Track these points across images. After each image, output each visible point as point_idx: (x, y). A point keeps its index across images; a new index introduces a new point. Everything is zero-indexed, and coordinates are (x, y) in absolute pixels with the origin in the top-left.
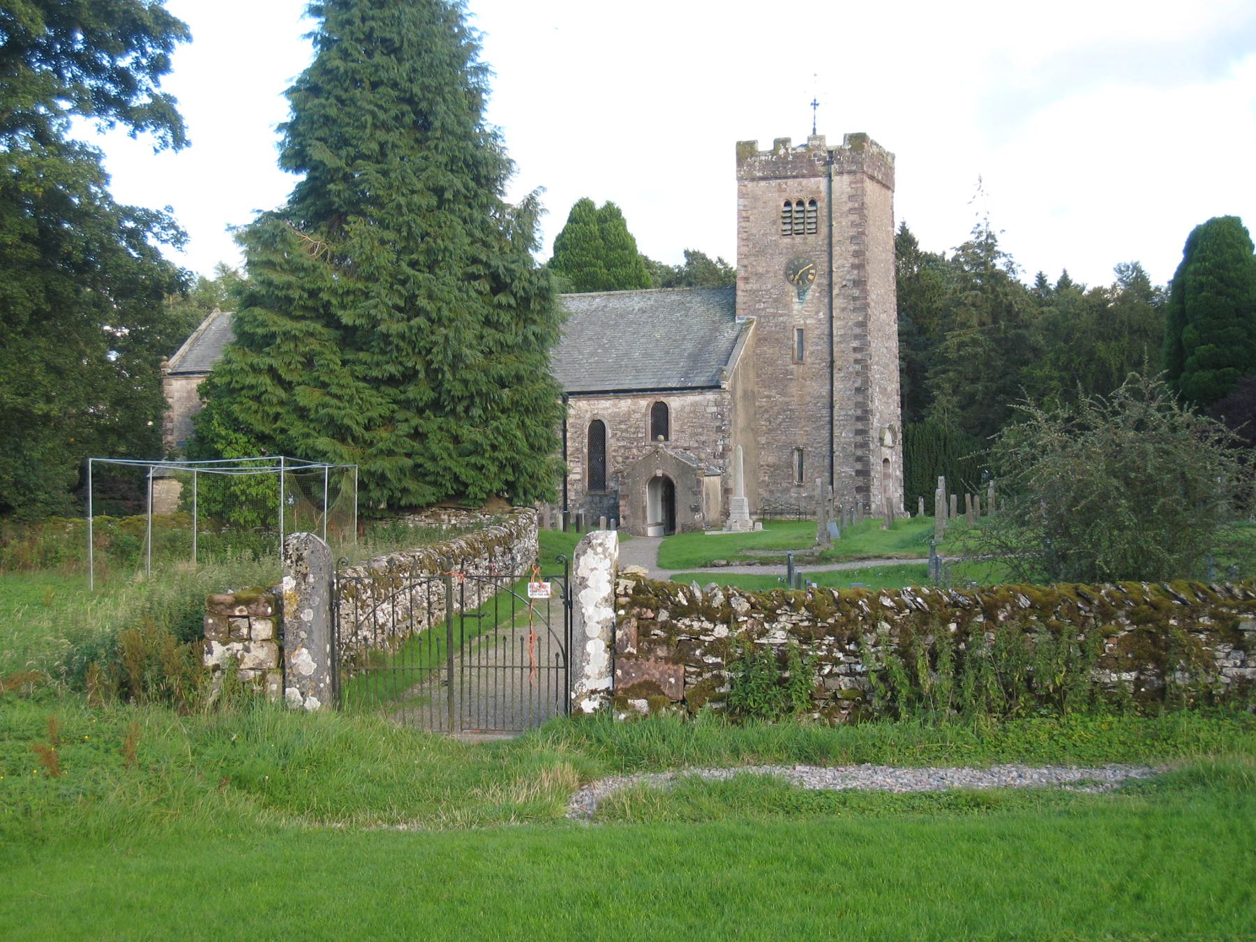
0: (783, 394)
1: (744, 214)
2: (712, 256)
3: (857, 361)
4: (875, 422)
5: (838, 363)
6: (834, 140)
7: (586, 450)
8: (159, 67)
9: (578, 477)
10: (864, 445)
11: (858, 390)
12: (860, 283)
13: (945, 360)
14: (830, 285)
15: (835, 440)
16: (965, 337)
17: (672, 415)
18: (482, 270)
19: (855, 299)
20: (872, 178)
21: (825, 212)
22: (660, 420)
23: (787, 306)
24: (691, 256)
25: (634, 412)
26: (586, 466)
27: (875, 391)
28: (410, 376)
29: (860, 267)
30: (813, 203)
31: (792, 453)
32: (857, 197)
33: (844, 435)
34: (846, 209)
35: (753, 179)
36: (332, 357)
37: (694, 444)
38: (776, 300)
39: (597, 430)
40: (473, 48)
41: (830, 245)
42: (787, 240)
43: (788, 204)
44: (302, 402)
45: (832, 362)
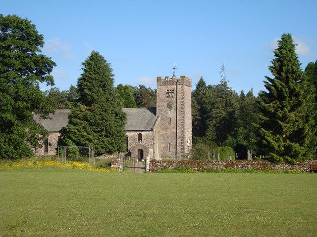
2: (147, 87)
4: (186, 138)
5: (178, 125)
6: (178, 77)
8: (49, 71)
10: (184, 143)
12: (183, 108)
13: (212, 117)
16: (219, 112)
17: (143, 136)
18: (114, 112)
20: (186, 85)
24: (142, 87)
27: (186, 131)
28: (102, 131)
29: (183, 105)
30: (173, 91)
32: (183, 90)
33: (179, 141)
36: (88, 127)
40: (111, 71)
43: (168, 91)
44: (83, 134)
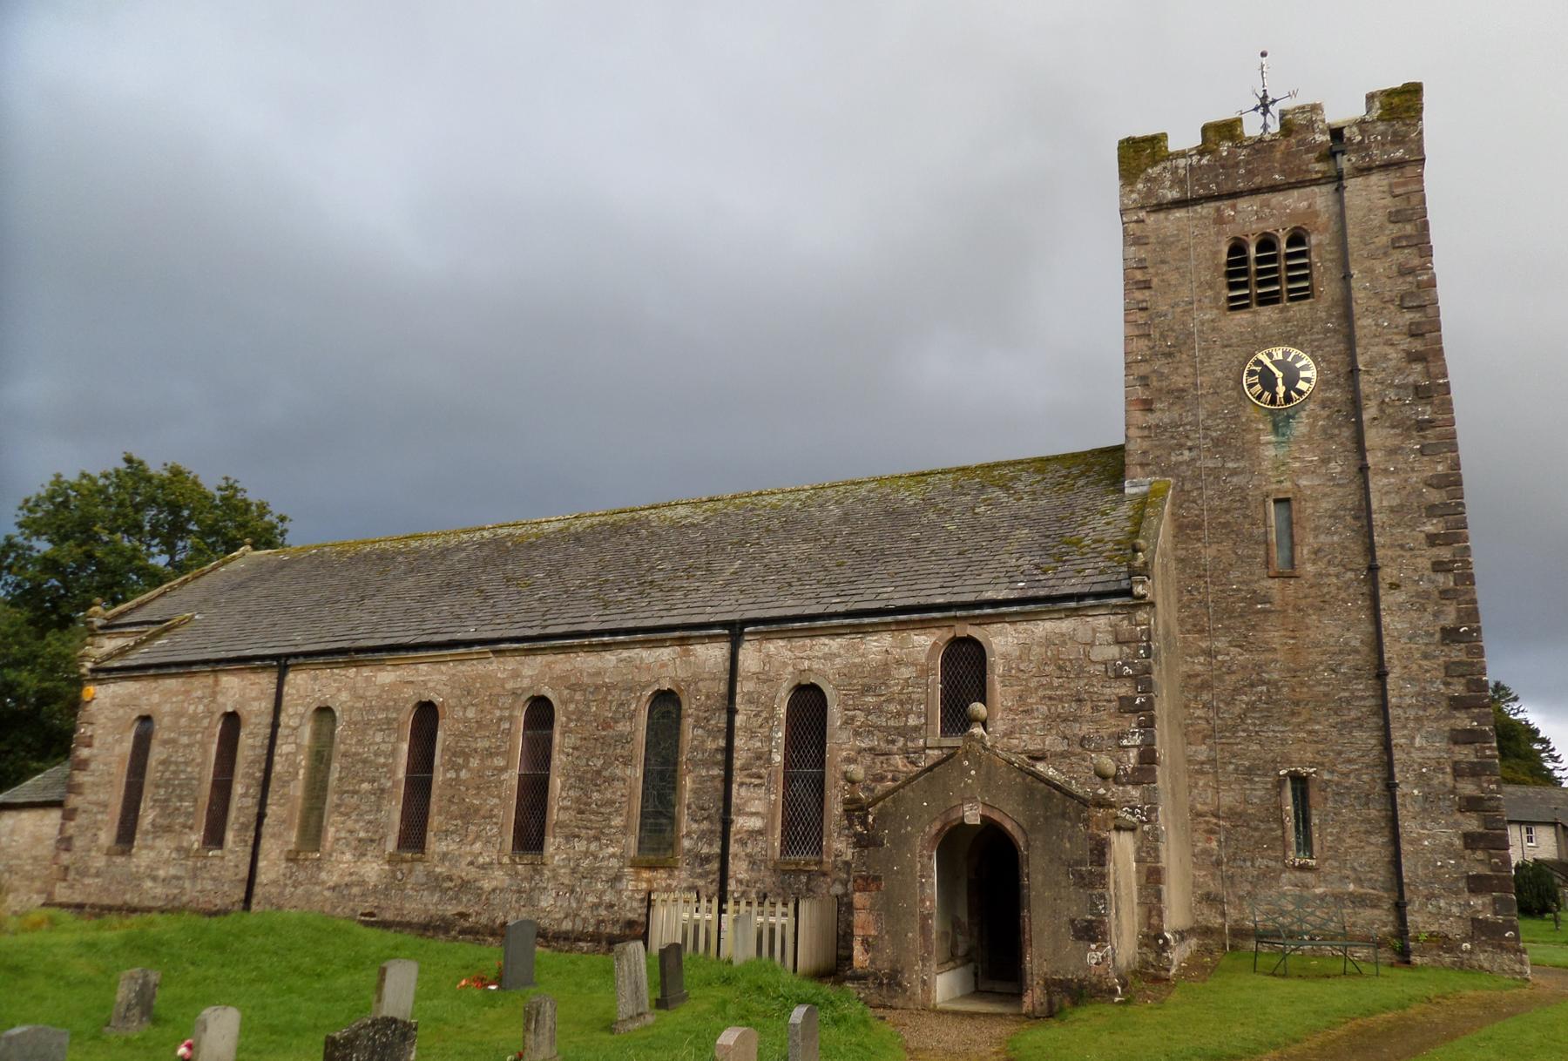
0: (1244, 645)
1: (1139, 275)
3: (1439, 566)
5: (1387, 574)
7: (778, 758)
9: (756, 823)
11: (1450, 635)
14: (1356, 405)
15: (1398, 755)
19: (1422, 426)
21: (1330, 252)
22: (965, 671)
23: (1248, 451)
25: (899, 663)
26: (777, 797)
30: (1297, 238)
31: (1280, 784)
34: (1383, 240)
35: (1160, 207)
37: (1053, 743)
38: (1217, 442)
39: (808, 705)
41: (1347, 316)
42: (1242, 317)
45: (1373, 569)
